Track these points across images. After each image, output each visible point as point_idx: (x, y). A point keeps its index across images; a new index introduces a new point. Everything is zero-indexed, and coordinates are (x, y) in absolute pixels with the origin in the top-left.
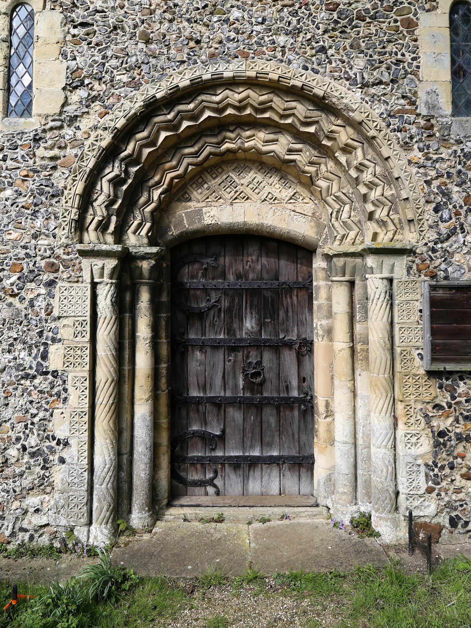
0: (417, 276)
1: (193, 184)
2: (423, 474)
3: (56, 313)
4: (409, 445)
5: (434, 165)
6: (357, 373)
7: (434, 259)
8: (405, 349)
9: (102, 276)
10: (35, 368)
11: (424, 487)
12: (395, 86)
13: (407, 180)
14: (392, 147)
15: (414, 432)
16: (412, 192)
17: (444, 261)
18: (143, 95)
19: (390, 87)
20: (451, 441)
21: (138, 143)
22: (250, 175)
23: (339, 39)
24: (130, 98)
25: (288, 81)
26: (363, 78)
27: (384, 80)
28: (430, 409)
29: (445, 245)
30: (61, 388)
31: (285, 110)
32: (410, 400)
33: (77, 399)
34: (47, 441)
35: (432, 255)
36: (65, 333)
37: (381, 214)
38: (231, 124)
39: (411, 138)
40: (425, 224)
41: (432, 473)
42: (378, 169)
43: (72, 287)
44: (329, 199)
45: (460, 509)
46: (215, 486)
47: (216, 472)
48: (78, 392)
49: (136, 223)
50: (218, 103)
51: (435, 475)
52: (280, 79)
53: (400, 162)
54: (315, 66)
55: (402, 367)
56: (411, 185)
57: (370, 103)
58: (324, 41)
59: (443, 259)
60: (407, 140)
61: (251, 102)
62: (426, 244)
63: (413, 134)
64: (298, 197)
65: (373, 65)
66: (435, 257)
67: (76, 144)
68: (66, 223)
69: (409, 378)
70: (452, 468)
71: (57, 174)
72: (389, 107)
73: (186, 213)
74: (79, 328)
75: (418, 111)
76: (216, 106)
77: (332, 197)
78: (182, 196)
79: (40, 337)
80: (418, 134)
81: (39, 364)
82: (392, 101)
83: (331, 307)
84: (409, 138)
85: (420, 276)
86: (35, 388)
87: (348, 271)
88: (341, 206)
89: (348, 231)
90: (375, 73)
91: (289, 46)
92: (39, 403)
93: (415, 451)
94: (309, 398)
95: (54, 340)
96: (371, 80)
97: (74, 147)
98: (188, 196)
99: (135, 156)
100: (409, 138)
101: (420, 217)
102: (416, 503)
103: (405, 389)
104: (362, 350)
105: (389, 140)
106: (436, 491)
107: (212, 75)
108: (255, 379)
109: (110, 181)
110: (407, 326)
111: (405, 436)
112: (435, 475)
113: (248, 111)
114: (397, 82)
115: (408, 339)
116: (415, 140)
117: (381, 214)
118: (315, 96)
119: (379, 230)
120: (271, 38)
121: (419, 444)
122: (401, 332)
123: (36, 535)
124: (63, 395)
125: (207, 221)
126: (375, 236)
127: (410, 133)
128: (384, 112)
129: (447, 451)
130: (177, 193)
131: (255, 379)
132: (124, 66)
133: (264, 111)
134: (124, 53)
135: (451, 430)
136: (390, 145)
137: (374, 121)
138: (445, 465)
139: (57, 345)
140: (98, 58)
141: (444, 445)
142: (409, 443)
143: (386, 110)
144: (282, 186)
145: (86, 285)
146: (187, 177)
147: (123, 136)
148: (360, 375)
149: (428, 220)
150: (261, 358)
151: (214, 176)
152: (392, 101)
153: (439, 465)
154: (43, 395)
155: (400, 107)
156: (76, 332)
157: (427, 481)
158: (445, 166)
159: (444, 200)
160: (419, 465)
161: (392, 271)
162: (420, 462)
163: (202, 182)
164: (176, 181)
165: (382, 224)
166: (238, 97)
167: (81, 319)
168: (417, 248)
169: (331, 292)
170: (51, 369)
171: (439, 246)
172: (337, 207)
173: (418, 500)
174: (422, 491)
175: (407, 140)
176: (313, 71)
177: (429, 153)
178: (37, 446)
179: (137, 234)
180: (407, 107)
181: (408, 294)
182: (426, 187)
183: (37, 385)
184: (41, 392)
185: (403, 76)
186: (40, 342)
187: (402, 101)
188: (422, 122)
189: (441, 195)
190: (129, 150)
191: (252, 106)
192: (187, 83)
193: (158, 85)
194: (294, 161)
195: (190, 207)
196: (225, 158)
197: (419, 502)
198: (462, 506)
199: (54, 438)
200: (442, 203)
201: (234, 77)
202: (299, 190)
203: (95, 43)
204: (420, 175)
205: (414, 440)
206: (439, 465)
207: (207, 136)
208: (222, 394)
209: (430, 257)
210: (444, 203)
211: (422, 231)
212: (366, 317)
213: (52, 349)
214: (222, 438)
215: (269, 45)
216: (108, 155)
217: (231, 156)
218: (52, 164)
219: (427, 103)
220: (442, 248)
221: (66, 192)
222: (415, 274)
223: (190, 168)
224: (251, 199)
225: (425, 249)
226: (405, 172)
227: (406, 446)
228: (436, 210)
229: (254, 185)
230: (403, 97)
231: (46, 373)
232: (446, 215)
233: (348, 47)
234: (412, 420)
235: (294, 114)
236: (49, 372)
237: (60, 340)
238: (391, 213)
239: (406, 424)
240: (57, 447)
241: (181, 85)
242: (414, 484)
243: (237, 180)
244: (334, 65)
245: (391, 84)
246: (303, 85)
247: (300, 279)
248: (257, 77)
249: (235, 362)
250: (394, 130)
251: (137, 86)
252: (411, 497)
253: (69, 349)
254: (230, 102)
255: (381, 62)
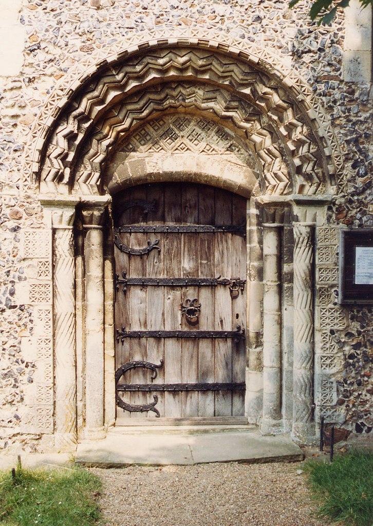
0: (336, 224)
1: (136, 135)
2: (335, 389)
3: (21, 254)
4: (324, 366)
5: (354, 127)
6: (284, 308)
7: (351, 209)
8: (324, 286)
9: (61, 221)
10: (4, 303)
11: (335, 399)
12: (322, 54)
13: (330, 140)
14: (317, 110)
15: (329, 355)
16: (334, 150)
17: (359, 211)
18: (95, 59)
19: (318, 55)
20: (359, 362)
21: (89, 101)
22: (190, 127)
23: (273, 9)
24: (84, 62)
25: (226, 48)
26: (294, 47)
27: (312, 49)
28: (343, 336)
29: (360, 197)
30: (27, 320)
31: (223, 72)
32: (326, 330)
33: (42, 329)
34: (16, 364)
35: (349, 206)
36: (29, 273)
37: (308, 168)
38: (174, 82)
39: (335, 102)
40: (345, 178)
41: (342, 389)
42: (305, 129)
43: (34, 232)
44: (262, 153)
45: (365, 417)
46: (156, 411)
47: (156, 398)
48: (43, 322)
49: (86, 173)
50: (162, 66)
51: (345, 390)
52: (220, 46)
53: (324, 123)
54: (251, 35)
55: (320, 302)
56: (333, 144)
57: (299, 69)
58: (259, 11)
59: (358, 210)
60: (331, 104)
61: (193, 65)
62: (344, 196)
63: (336, 98)
64: (234, 148)
65: (303, 35)
66: (352, 207)
67: (35, 104)
68: (28, 175)
69: (326, 311)
70: (359, 384)
71: (17, 131)
72: (316, 73)
73: (130, 163)
74: (43, 269)
75: (341, 78)
76: (160, 68)
77: (265, 150)
78: (126, 147)
79: (8, 276)
80: (341, 99)
81: (8, 300)
82: (319, 68)
83: (262, 249)
84: (332, 102)
85: (338, 224)
86: (5, 319)
87: (277, 217)
88: (273, 160)
89: (278, 182)
90: (304, 42)
91: (228, 15)
92: (8, 332)
93: (329, 371)
94: (241, 332)
95: (20, 278)
96: (300, 49)
97: (33, 106)
98: (131, 147)
99: (86, 114)
100: (332, 102)
101: (340, 173)
102: (329, 413)
103: (322, 320)
104: (288, 288)
105: (315, 104)
106: (346, 404)
107: (158, 41)
108: (191, 313)
109: (65, 137)
110: (326, 267)
111: (322, 359)
112: (345, 390)
113: (190, 73)
114: (324, 51)
115: (332, 277)
116: (338, 104)
117: (308, 168)
118: (251, 62)
119: (305, 183)
120: (211, 7)
121: (333, 365)
122: (320, 272)
123: (10, 442)
124: (30, 325)
125: (150, 169)
126: (302, 187)
127: (334, 97)
128: (312, 78)
129: (356, 370)
130: (121, 146)
131: (191, 313)
132: (77, 31)
133: (204, 72)
134: (77, 19)
135: (359, 353)
136: (316, 108)
137: (302, 87)
138: (354, 382)
139: (23, 283)
140: (54, 23)
141: (354, 365)
142: (324, 364)
143: (313, 76)
144: (219, 137)
145: (48, 231)
146: (131, 129)
147: (76, 96)
148: (286, 309)
149: (347, 175)
150: (198, 296)
151: (156, 128)
152: (319, 68)
153: (348, 382)
154: (12, 326)
155: (326, 74)
156: (40, 272)
157: (338, 395)
158: (364, 127)
159: (361, 158)
160: (332, 383)
161: (314, 220)
162: (333, 379)
163: (144, 134)
164: (122, 134)
165: (309, 177)
166: (182, 60)
167: (44, 260)
168: (336, 200)
169: (262, 236)
170: (18, 304)
171: (356, 198)
172: (269, 160)
173: (330, 411)
174: (334, 403)
175: (331, 104)
176: (249, 40)
177: (350, 115)
178: (8, 368)
179: (87, 183)
180: (332, 74)
181: (327, 240)
182: (346, 145)
183: (7, 317)
184: (10, 323)
185: (330, 45)
186: (8, 281)
187: (328, 69)
188: (345, 88)
189: (359, 154)
190: (81, 109)
191: (194, 69)
192: (136, 48)
193: (109, 50)
194: (231, 117)
195: (134, 157)
196: (167, 112)
197: (331, 412)
198: (366, 415)
199: (23, 362)
200: (359, 160)
201: (178, 43)
202: (234, 142)
203: (51, 9)
204: (341, 135)
205: (328, 362)
206: (348, 382)
207: (151, 93)
208: (162, 329)
209: (347, 207)
210: (361, 160)
211: (341, 185)
212: (291, 260)
213: (18, 287)
214: (162, 367)
215: (210, 14)
216: (63, 115)
217: (172, 110)
218: (13, 121)
219: (349, 71)
220: (358, 200)
221: (26, 147)
222: (334, 222)
223: (135, 122)
224: (190, 150)
225: (343, 200)
226: (329, 132)
227: (322, 367)
228: (354, 167)
229: (193, 136)
230: (330, 65)
231: (15, 307)
232: (362, 171)
233: (281, 17)
234: (328, 346)
235: (231, 76)
236: (17, 306)
237: (25, 279)
238: (316, 167)
239: (322, 349)
240: (26, 369)
241: (130, 50)
242: (328, 397)
243: (177, 132)
244: (268, 33)
245: (318, 52)
246: (240, 52)
247: (234, 223)
248: (198, 43)
249: (174, 300)
250: (320, 95)
251: (90, 50)
252: (324, 408)
253: (34, 286)
254: (173, 65)
255: (310, 32)
